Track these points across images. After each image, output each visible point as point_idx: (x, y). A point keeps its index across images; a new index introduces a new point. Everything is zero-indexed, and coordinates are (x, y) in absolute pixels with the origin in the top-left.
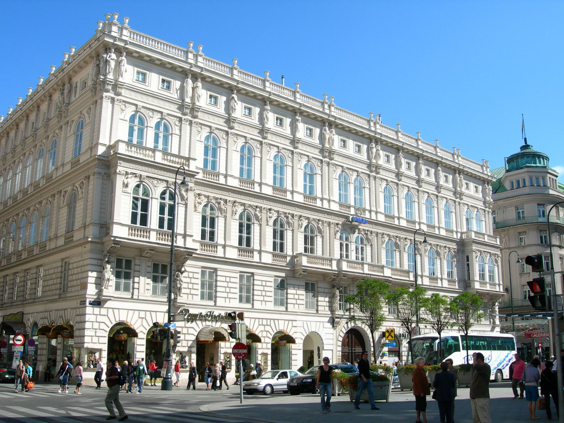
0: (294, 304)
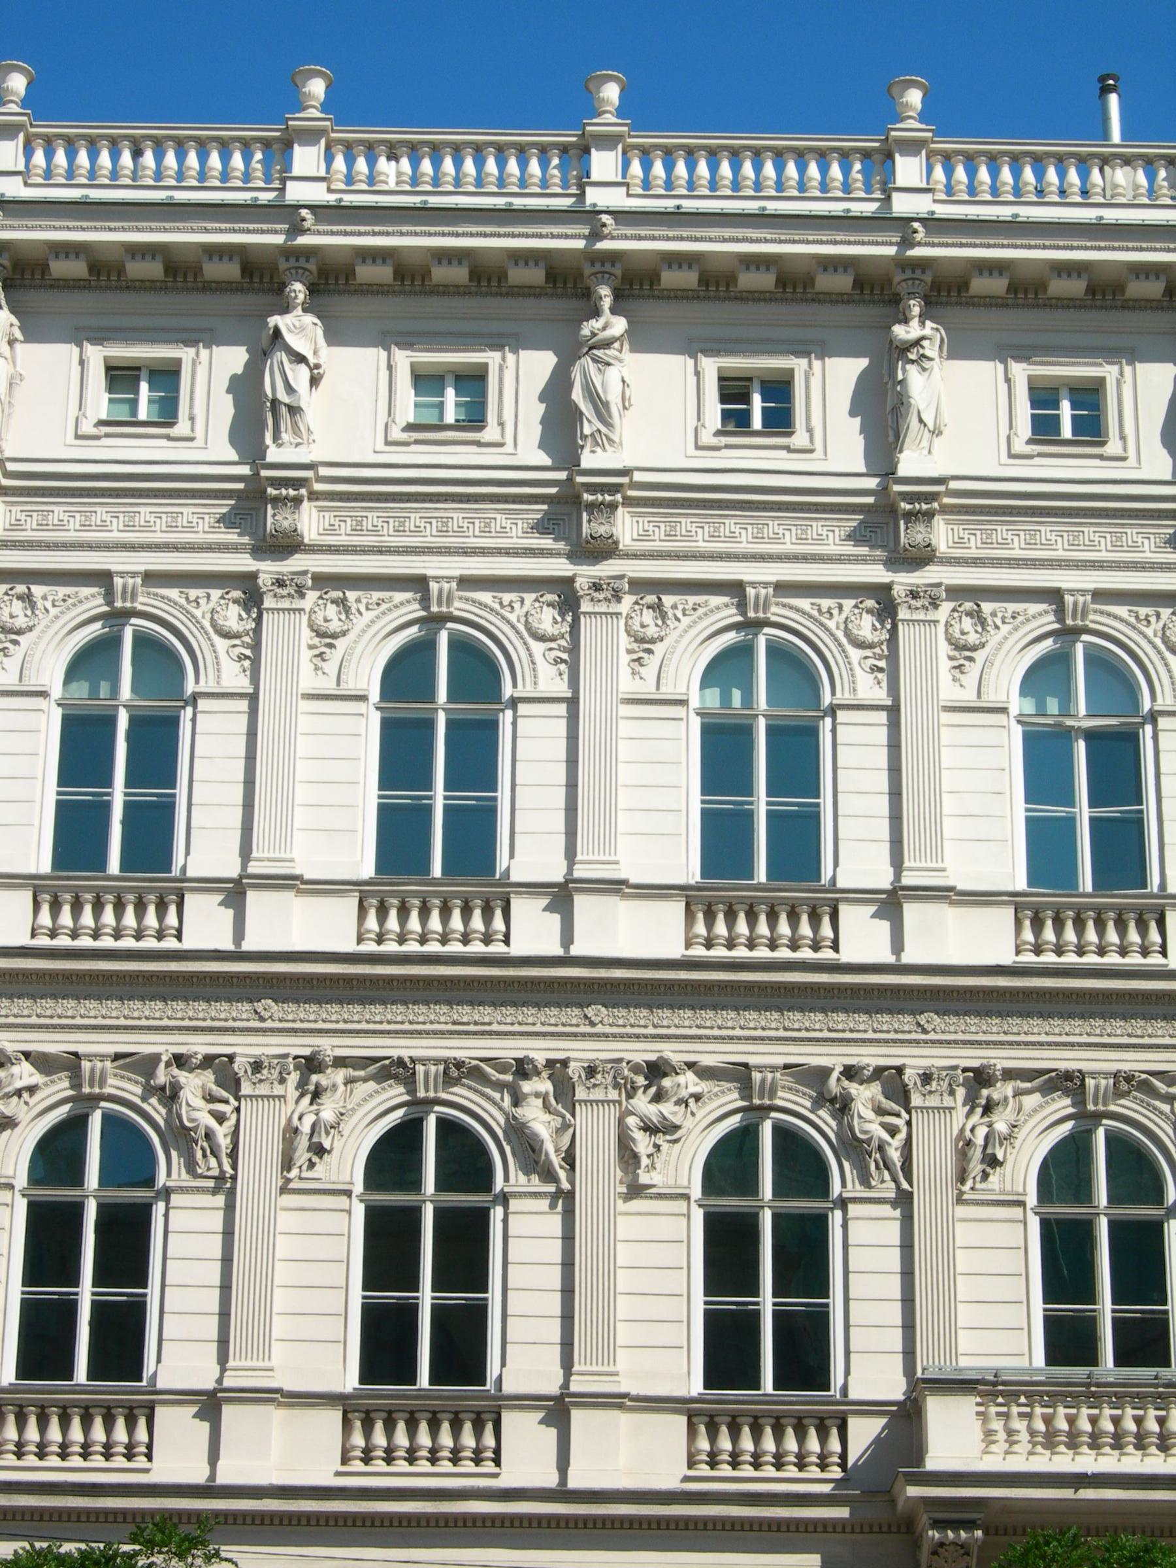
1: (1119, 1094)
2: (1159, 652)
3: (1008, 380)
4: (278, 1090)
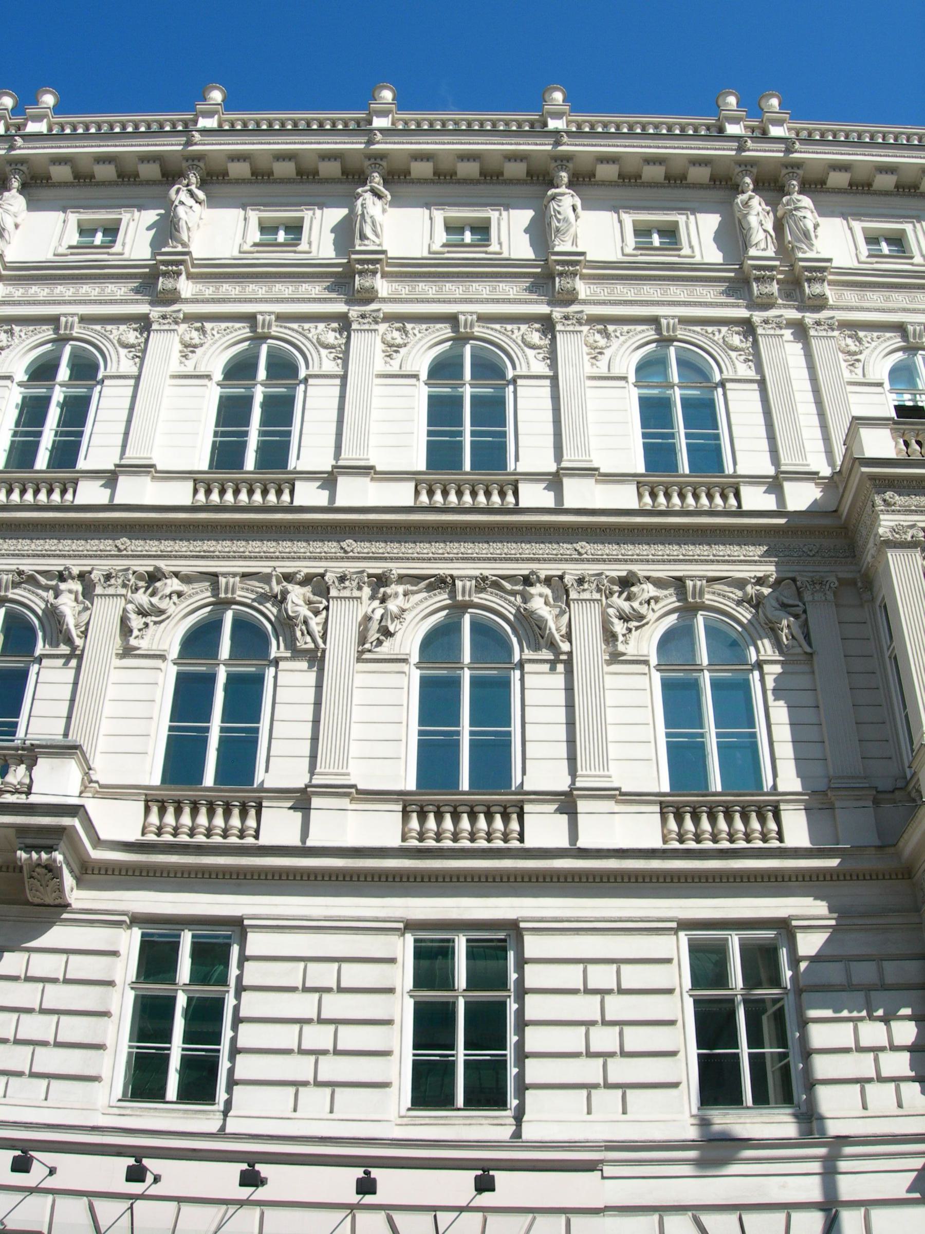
0: (862, 1081)
1: (16, 585)
4: (356, 593)
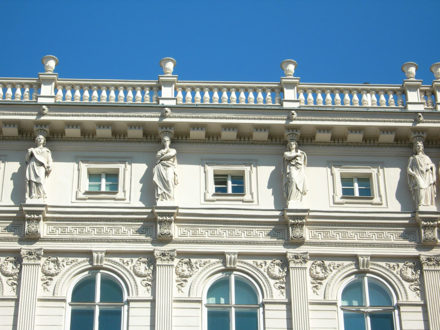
2: (399, 280)
3: (332, 174)
